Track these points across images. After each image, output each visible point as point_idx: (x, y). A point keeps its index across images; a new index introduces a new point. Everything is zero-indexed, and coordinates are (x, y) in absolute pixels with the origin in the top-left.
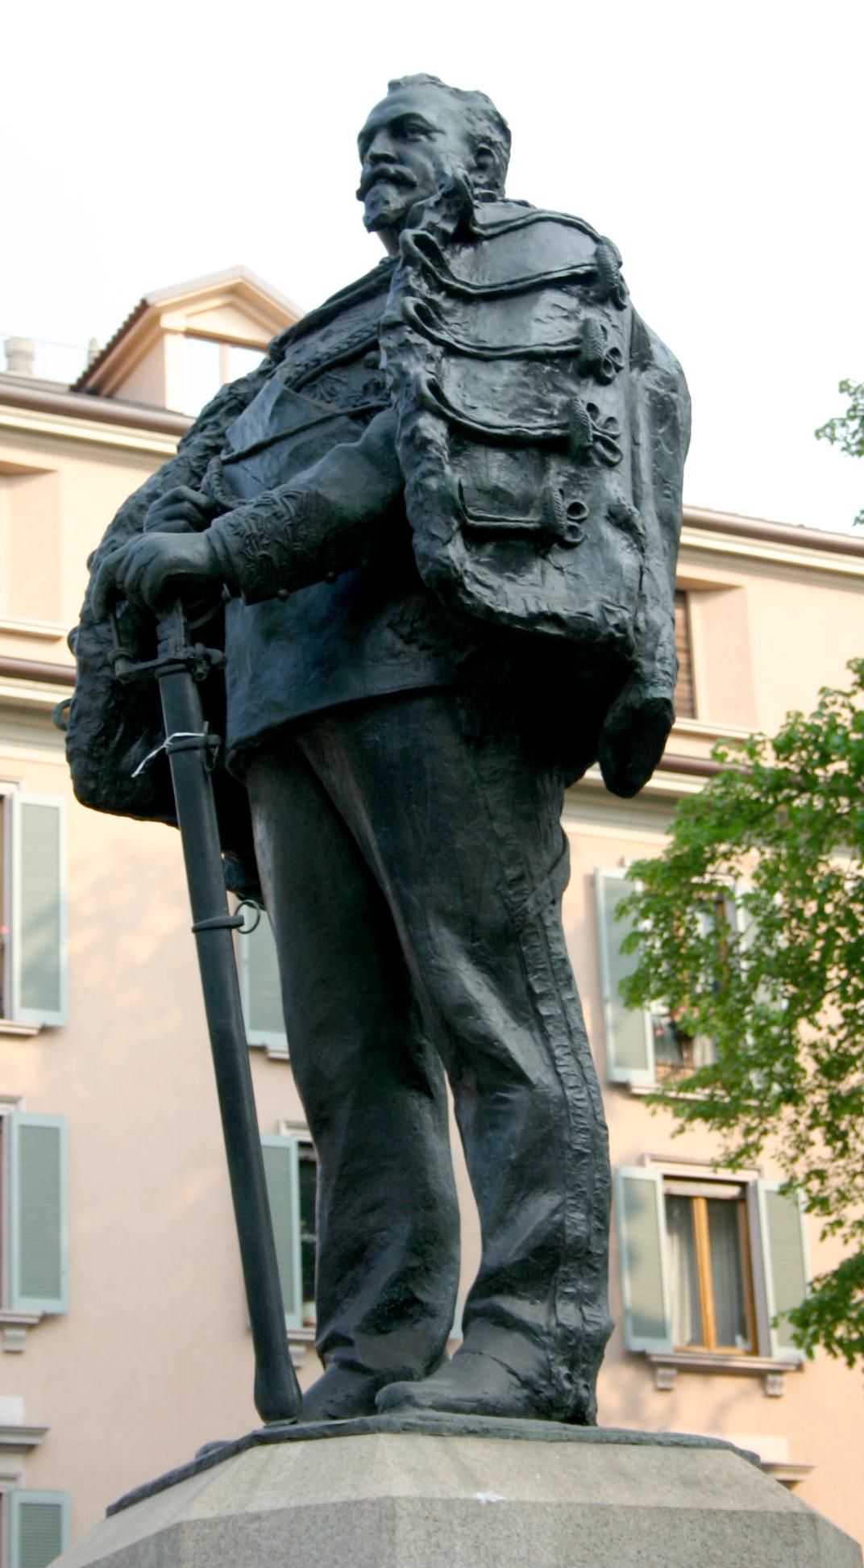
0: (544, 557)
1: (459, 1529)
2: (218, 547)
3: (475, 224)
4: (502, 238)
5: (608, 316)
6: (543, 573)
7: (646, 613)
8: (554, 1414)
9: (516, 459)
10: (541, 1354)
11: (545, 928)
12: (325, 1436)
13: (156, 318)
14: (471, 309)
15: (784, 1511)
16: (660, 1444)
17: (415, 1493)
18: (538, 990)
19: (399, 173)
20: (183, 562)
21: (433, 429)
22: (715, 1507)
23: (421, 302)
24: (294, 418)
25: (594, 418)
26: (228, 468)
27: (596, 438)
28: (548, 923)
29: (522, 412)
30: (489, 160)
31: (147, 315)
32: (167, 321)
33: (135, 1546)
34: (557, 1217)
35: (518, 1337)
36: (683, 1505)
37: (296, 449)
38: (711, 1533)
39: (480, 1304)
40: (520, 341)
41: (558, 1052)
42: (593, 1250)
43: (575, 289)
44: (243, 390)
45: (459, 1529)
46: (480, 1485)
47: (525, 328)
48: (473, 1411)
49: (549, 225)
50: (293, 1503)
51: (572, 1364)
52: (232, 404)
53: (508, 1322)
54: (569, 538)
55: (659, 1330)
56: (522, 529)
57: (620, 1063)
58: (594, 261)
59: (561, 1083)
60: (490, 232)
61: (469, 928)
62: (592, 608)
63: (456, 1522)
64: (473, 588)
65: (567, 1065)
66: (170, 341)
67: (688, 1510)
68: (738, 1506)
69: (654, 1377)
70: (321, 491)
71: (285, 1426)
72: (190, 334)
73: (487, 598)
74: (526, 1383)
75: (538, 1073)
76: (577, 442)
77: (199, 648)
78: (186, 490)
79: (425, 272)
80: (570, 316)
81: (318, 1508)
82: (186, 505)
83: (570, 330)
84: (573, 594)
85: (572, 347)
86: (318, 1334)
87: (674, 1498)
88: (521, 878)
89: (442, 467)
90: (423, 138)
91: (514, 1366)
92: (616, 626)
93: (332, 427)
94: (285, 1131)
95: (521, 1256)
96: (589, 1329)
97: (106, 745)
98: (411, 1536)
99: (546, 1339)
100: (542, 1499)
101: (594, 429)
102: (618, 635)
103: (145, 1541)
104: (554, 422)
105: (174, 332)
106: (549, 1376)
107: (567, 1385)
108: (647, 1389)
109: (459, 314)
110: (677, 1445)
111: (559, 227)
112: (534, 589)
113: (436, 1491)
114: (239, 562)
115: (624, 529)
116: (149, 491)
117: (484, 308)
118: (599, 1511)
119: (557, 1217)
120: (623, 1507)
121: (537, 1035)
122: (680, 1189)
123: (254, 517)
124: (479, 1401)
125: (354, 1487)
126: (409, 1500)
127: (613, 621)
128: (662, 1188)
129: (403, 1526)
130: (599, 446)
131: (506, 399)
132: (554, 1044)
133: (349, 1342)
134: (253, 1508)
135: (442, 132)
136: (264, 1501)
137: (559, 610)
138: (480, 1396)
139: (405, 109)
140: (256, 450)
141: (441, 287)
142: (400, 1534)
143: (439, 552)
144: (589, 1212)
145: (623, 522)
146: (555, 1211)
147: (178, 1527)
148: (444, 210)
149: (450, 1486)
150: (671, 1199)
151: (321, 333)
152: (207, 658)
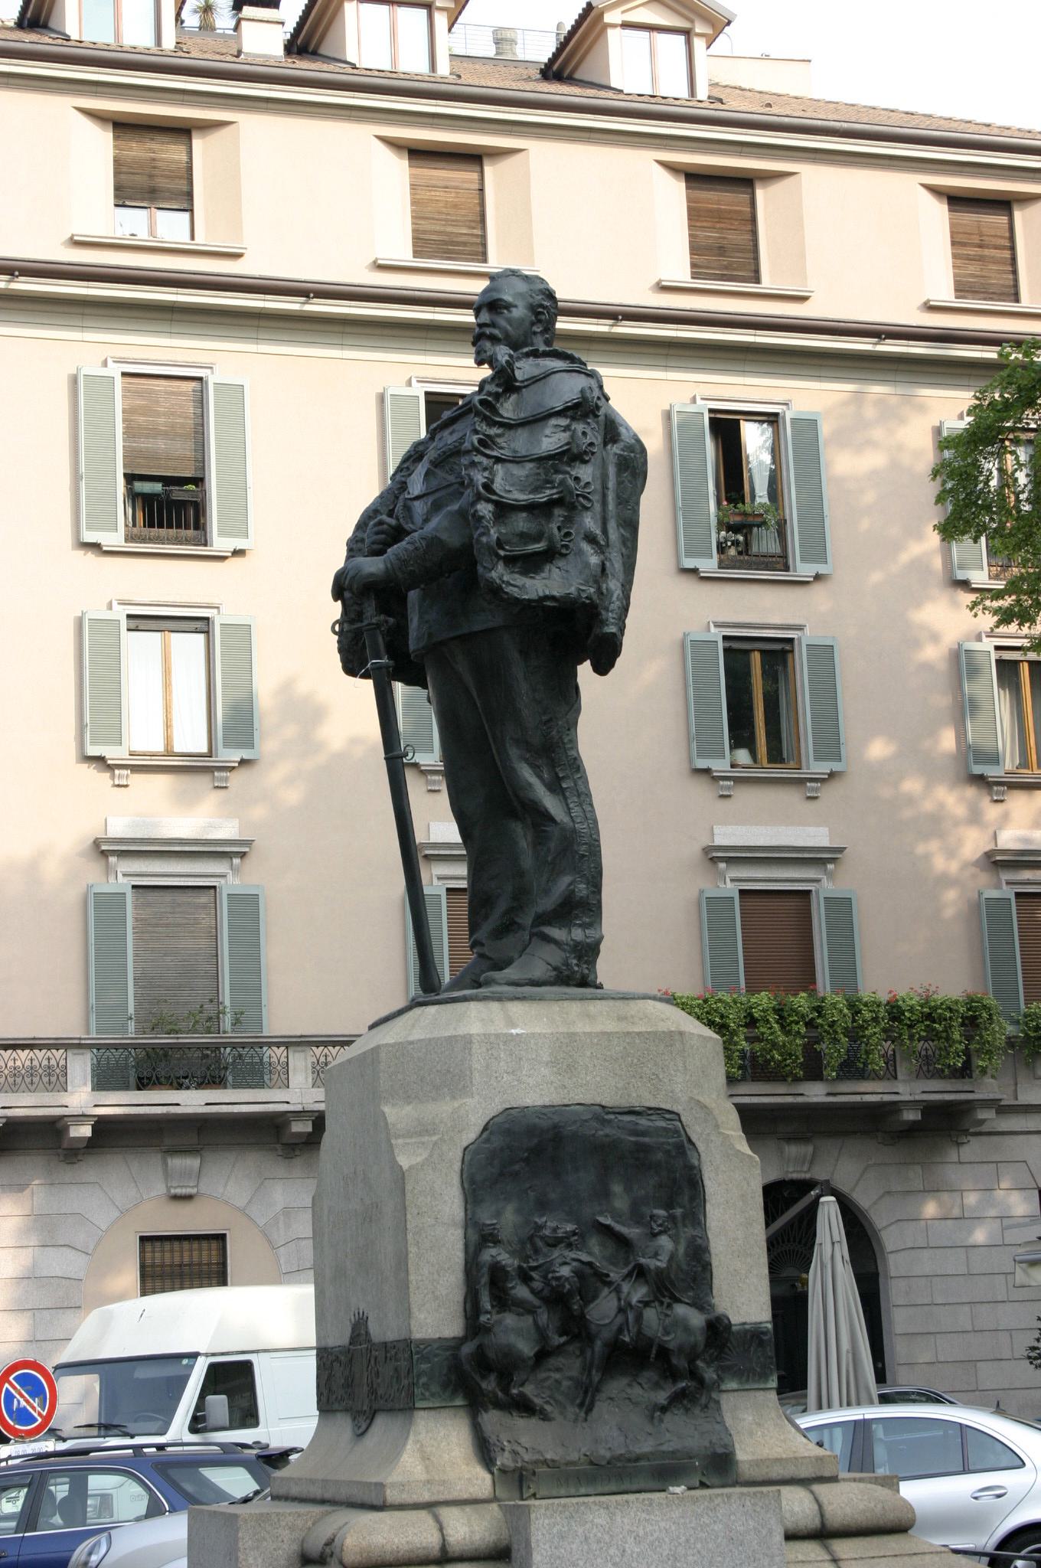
0: (551, 562)
1: (502, 1047)
2: (389, 565)
3: (516, 381)
4: (532, 387)
5: (589, 423)
6: (550, 571)
7: (607, 584)
8: (571, 983)
9: (533, 514)
10: (563, 954)
11: (564, 743)
12: (447, 1002)
13: (601, 15)
14: (512, 433)
15: (665, 1030)
16: (613, 998)
17: (482, 1031)
18: (561, 775)
19: (491, 334)
20: (372, 575)
21: (485, 509)
22: (631, 1030)
23: (481, 436)
24: (434, 483)
25: (578, 484)
26: (409, 503)
27: (578, 495)
28: (566, 741)
29: (536, 490)
30: (543, 317)
31: (593, 14)
32: (609, 18)
33: (364, 1053)
34: (572, 887)
35: (553, 946)
36: (616, 1030)
37: (435, 501)
38: (628, 1043)
39: (535, 930)
40: (536, 451)
41: (571, 806)
42: (591, 902)
43: (569, 413)
44: (421, 448)
45: (502, 1047)
46: (514, 1026)
47: (539, 442)
48: (527, 984)
49: (558, 376)
50: (428, 1036)
51: (579, 958)
52: (415, 457)
53: (547, 939)
54: (564, 551)
55: (995, 759)
56: (535, 552)
57: (961, 567)
58: (580, 396)
59: (573, 821)
60: (526, 383)
61: (525, 744)
62: (573, 590)
63: (501, 1044)
64: (509, 589)
65: (576, 811)
66: (613, 35)
67: (617, 1033)
68: (643, 1029)
69: (990, 794)
70: (438, 535)
71: (433, 997)
72: (626, 25)
73: (514, 592)
74: (555, 969)
75: (561, 817)
76: (568, 499)
77: (382, 617)
78: (384, 517)
79: (485, 419)
80: (567, 428)
81: (438, 1039)
82: (385, 526)
83: (564, 437)
84: (565, 581)
85: (565, 448)
86: (470, 939)
87: (611, 1026)
88: (550, 720)
89: (489, 531)
90: (505, 311)
91: (550, 961)
92: (587, 598)
93: (451, 489)
94: (713, 629)
95: (553, 906)
96: (588, 941)
97: (357, 644)
98: (479, 1051)
99: (566, 947)
100: (544, 1031)
101: (577, 490)
102: (588, 601)
103: (368, 1051)
104: (555, 491)
105: (614, 26)
106: (567, 964)
107: (576, 969)
108: (985, 802)
109: (506, 436)
110: (623, 998)
111: (564, 374)
112: (544, 581)
113: (492, 1030)
114: (400, 574)
115: (593, 544)
116: (374, 508)
117: (520, 431)
118: (572, 1036)
119: (572, 887)
120: (584, 1033)
121: (561, 798)
122: (1008, 656)
123: (406, 550)
124: (530, 979)
125: (455, 1029)
126: (478, 1035)
127: (584, 595)
128: (994, 656)
129: (475, 1046)
130: (581, 499)
131: (527, 484)
132: (569, 801)
133: (483, 945)
134: (411, 1038)
135: (516, 306)
136: (417, 1035)
137: (555, 593)
138: (530, 976)
139: (496, 296)
140: (417, 498)
141: (492, 424)
142: (474, 1051)
143: (488, 575)
144: (588, 884)
145: (591, 539)
146: (570, 884)
147: (378, 1047)
148: (497, 381)
149: (499, 1027)
150: (999, 662)
151: (451, 429)
152: (387, 622)
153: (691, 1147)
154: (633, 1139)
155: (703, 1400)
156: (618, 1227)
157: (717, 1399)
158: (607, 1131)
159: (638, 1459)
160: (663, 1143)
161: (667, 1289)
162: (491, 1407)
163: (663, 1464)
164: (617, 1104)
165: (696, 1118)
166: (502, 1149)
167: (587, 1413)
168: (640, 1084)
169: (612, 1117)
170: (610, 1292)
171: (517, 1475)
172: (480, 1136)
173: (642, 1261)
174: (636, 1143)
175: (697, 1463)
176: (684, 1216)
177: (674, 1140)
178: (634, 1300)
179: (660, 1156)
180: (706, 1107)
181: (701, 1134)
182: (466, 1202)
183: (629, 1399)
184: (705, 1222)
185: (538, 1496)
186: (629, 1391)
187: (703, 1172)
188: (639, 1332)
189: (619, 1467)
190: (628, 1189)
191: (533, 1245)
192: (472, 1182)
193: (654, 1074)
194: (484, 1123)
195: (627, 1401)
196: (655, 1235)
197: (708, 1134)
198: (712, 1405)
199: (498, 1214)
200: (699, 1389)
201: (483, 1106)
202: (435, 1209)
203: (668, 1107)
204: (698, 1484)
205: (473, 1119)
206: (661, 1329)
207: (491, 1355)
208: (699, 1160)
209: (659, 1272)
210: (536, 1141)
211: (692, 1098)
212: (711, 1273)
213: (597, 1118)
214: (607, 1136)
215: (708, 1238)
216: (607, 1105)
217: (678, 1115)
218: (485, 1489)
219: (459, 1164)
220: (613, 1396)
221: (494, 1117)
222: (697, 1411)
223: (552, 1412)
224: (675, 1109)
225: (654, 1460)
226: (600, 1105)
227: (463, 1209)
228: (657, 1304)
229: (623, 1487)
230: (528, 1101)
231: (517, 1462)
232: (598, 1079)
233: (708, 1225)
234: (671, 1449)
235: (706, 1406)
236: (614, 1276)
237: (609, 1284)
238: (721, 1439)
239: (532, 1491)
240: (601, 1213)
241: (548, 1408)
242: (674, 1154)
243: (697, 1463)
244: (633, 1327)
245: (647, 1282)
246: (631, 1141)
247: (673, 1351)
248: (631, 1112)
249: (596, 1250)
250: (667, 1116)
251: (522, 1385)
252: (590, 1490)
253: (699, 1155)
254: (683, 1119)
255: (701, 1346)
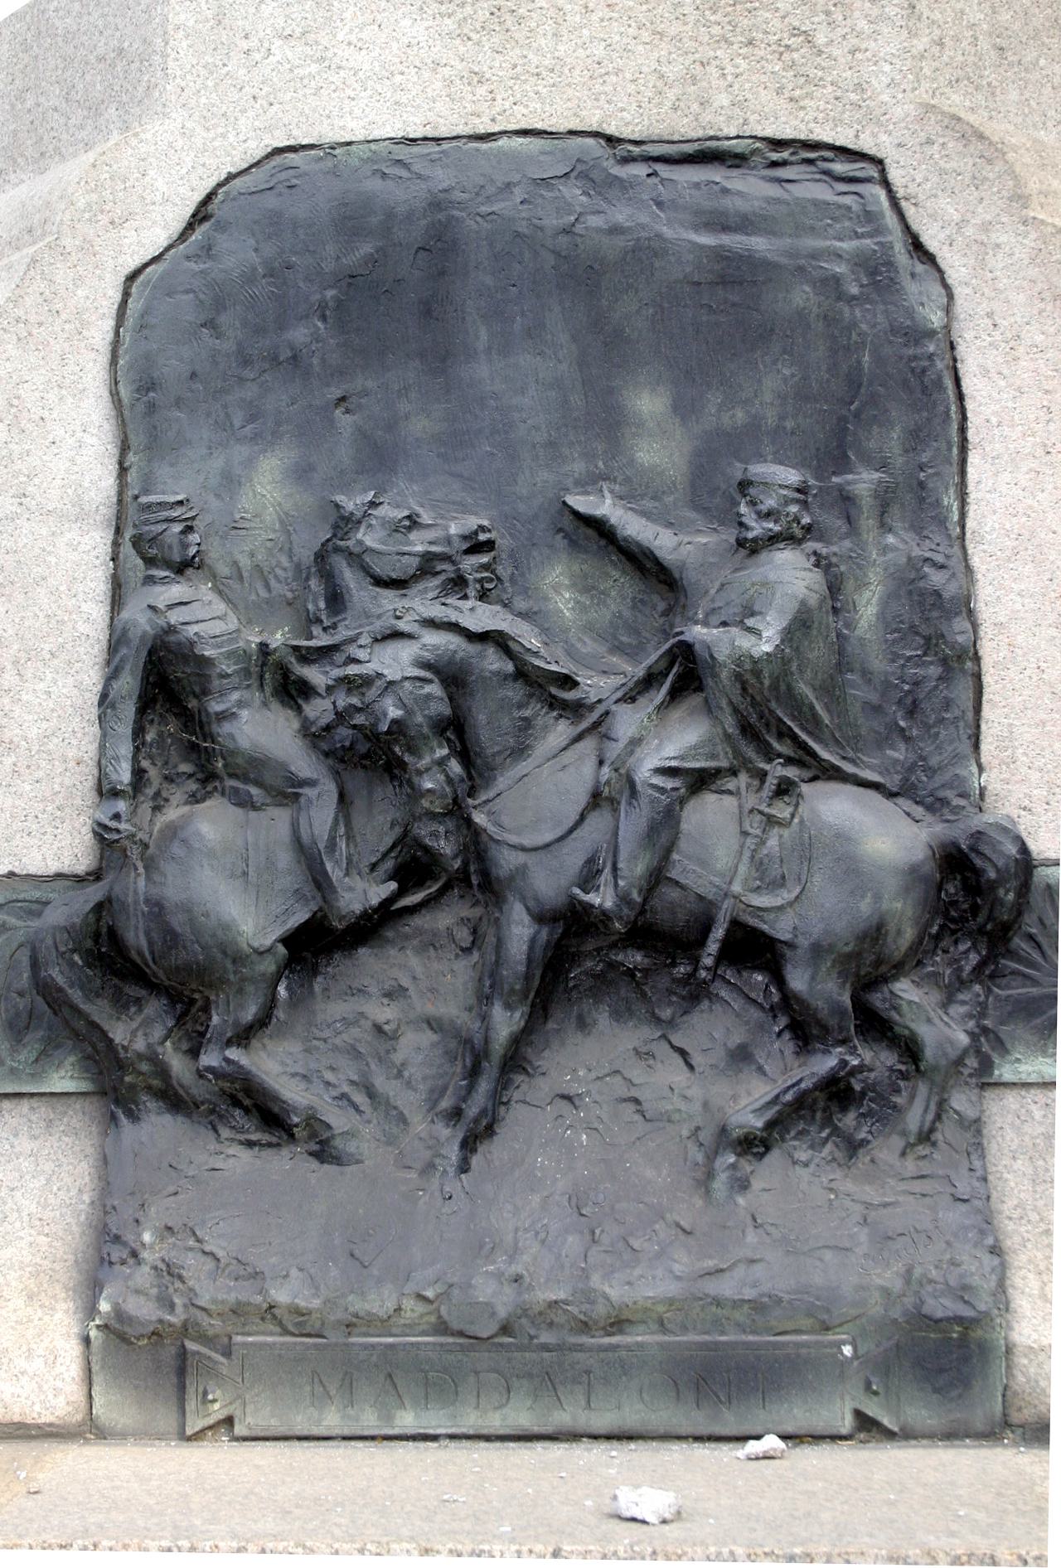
12: (582, 132)
153: (920, 268)
154: (706, 239)
155: (915, 1117)
156: (633, 526)
157: (971, 1113)
158: (621, 215)
159: (618, 1324)
160: (815, 255)
161: (785, 734)
162: (152, 1104)
163: (717, 1345)
164: (658, 130)
165: (942, 172)
166: (249, 278)
167: (469, 1145)
168: (743, 65)
169: (641, 170)
170: (579, 738)
171: (169, 1352)
172: (183, 236)
173: (697, 633)
174: (720, 255)
175: (847, 1350)
176: (884, 501)
177: (855, 243)
178: (645, 768)
179: (802, 296)
180: (981, 137)
181: (961, 225)
182: (124, 448)
183: (637, 1101)
184: (963, 515)
185: (239, 1430)
186: (636, 1073)
187: (962, 350)
188: (657, 877)
189: (545, 1348)
190: (684, 409)
191: (328, 577)
192: (147, 385)
193: (796, 32)
194: (199, 196)
195: (631, 1108)
196: (751, 548)
197: (986, 227)
198: (947, 1132)
199: (230, 482)
200: (904, 1076)
201: (198, 142)
202: (18, 465)
203: (843, 138)
204: (847, 1424)
205: (160, 184)
206: (743, 869)
207: (136, 937)
208: (948, 310)
209: (748, 673)
210: (366, 248)
211: (930, 108)
212: (978, 677)
213: (584, 176)
214: (615, 230)
215: (969, 570)
216: (626, 133)
217: (879, 162)
218: (57, 1392)
219: (110, 323)
220: (575, 1089)
221: (231, 177)
222: (886, 1150)
223: (350, 1134)
224: (866, 144)
225: (685, 1329)
226: (596, 135)
227: (113, 467)
228: (743, 779)
229: (562, 1418)
230: (351, 124)
231: (172, 1307)
232: (599, 51)
233: (970, 524)
234: (749, 1293)
235: (926, 1137)
236: (595, 685)
237: (576, 710)
238: (954, 1263)
239: (217, 1411)
240: (590, 482)
241: (337, 1119)
242: (854, 290)
243: (847, 1350)
244: (634, 858)
245: (709, 709)
246: (702, 247)
247: (791, 945)
248: (708, 155)
249: (564, 603)
250: (839, 167)
251: (244, 1036)
252: (435, 1421)
253: (950, 296)
254: (895, 175)
255: (905, 936)
